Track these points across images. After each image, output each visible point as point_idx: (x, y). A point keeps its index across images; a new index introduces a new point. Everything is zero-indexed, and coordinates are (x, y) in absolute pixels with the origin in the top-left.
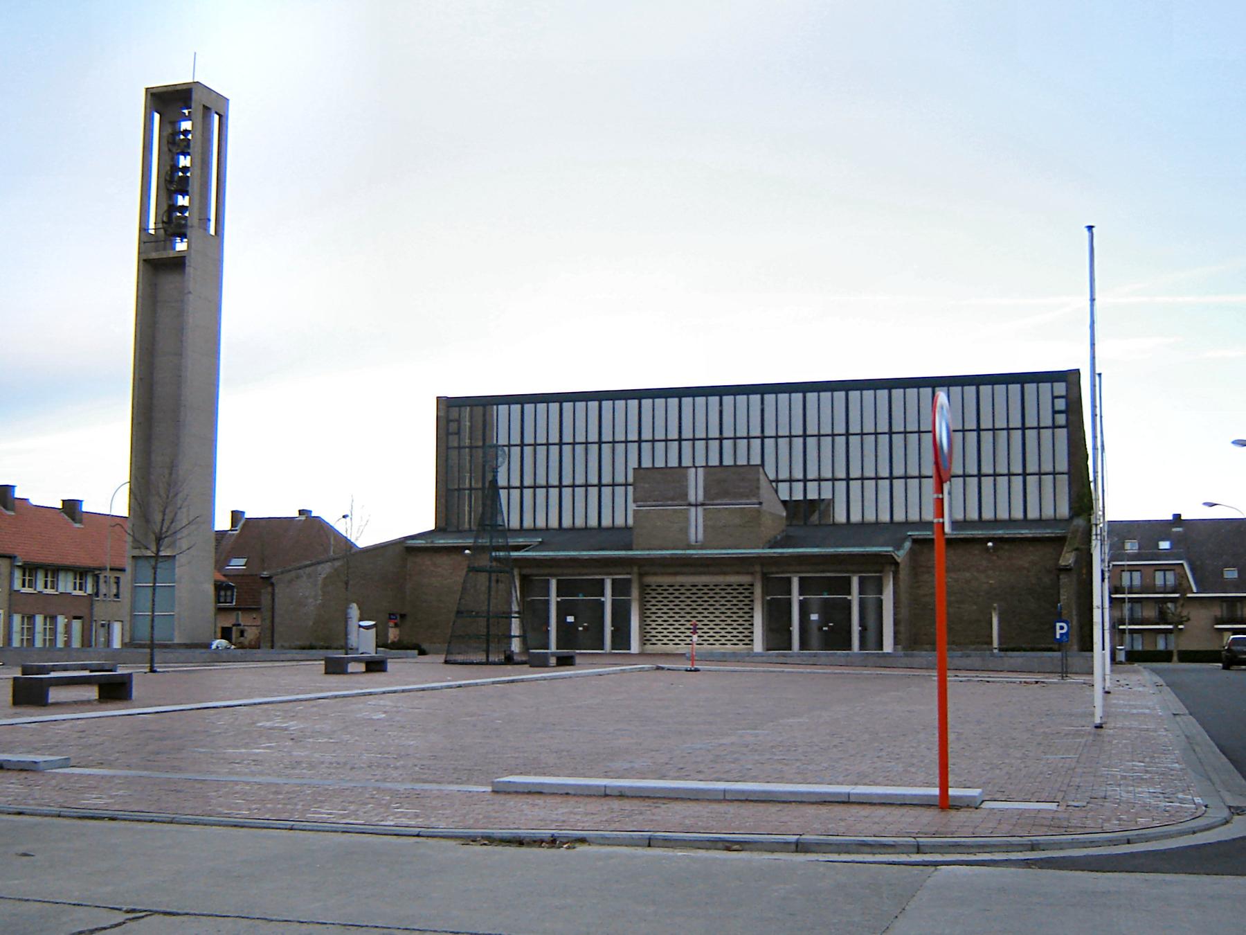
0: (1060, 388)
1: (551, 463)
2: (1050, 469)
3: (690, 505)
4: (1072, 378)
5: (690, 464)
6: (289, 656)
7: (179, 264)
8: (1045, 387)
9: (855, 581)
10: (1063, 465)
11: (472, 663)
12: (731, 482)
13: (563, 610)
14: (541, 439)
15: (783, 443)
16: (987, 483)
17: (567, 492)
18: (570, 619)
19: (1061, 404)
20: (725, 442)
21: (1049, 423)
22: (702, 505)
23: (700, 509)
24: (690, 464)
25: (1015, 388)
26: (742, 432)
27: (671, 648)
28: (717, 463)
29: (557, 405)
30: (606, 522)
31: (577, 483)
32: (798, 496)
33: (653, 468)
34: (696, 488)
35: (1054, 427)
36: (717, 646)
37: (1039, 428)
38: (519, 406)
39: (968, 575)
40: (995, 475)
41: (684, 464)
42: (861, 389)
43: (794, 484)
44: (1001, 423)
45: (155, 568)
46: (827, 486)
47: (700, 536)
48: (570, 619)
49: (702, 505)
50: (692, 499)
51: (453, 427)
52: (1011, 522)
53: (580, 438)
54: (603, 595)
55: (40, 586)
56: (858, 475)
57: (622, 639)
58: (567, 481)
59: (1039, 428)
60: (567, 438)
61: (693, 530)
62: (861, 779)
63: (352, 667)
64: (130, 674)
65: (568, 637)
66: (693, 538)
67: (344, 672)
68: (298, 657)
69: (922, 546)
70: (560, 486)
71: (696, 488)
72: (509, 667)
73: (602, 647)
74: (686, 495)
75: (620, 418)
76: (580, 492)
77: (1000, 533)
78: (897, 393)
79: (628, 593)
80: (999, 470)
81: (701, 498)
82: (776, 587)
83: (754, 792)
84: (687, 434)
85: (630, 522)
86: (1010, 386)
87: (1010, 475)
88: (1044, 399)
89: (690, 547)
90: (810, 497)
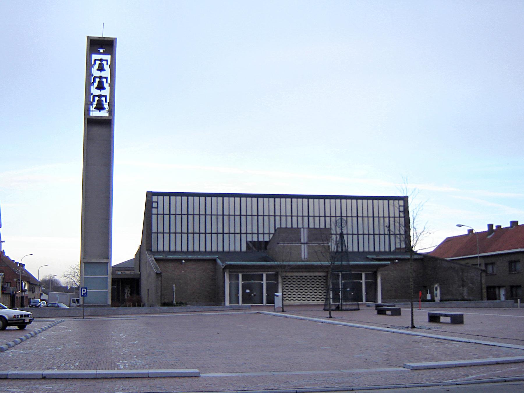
0: (402, 203)
1: (271, 225)
2: (180, 231)
3: (302, 243)
5: (301, 227)
6: (192, 310)
9: (240, 276)
10: (402, 232)
11: (348, 310)
12: (319, 235)
13: (244, 287)
15: (249, 218)
17: (377, 237)
18: (248, 291)
19: (402, 209)
20: (213, 216)
21: (398, 216)
22: (307, 243)
23: (305, 245)
24: (301, 227)
25: (272, 200)
26: (283, 213)
27: (292, 302)
28: (324, 227)
29: (186, 197)
30: (226, 249)
31: (213, 232)
32: (255, 239)
33: (281, 228)
34: (304, 236)
35: (400, 217)
36: (316, 301)
37: (314, 216)
38: (186, 197)
39: (387, 272)
40: (379, 234)
41: (299, 227)
42: (330, 199)
43: (254, 235)
44: (317, 214)
46: (249, 236)
47: (306, 257)
48: (248, 291)
49: (307, 243)
50: (302, 241)
52: (199, 252)
54: (361, 280)
56: (210, 231)
57: (271, 300)
58: (208, 231)
60: (208, 212)
61: (303, 254)
62: (173, 366)
63: (388, 312)
64: (463, 315)
65: (247, 299)
66: (303, 256)
67: (385, 314)
68: (197, 310)
69: (341, 263)
70: (374, 234)
71: (304, 236)
72: (337, 312)
73: (262, 303)
74: (300, 240)
75: (266, 205)
77: (190, 257)
78: (226, 199)
80: (183, 231)
81: (306, 241)
83: (125, 374)
85: (244, 249)
86: (183, 197)
87: (200, 233)
88: (395, 208)
89: (302, 261)
90: (260, 240)
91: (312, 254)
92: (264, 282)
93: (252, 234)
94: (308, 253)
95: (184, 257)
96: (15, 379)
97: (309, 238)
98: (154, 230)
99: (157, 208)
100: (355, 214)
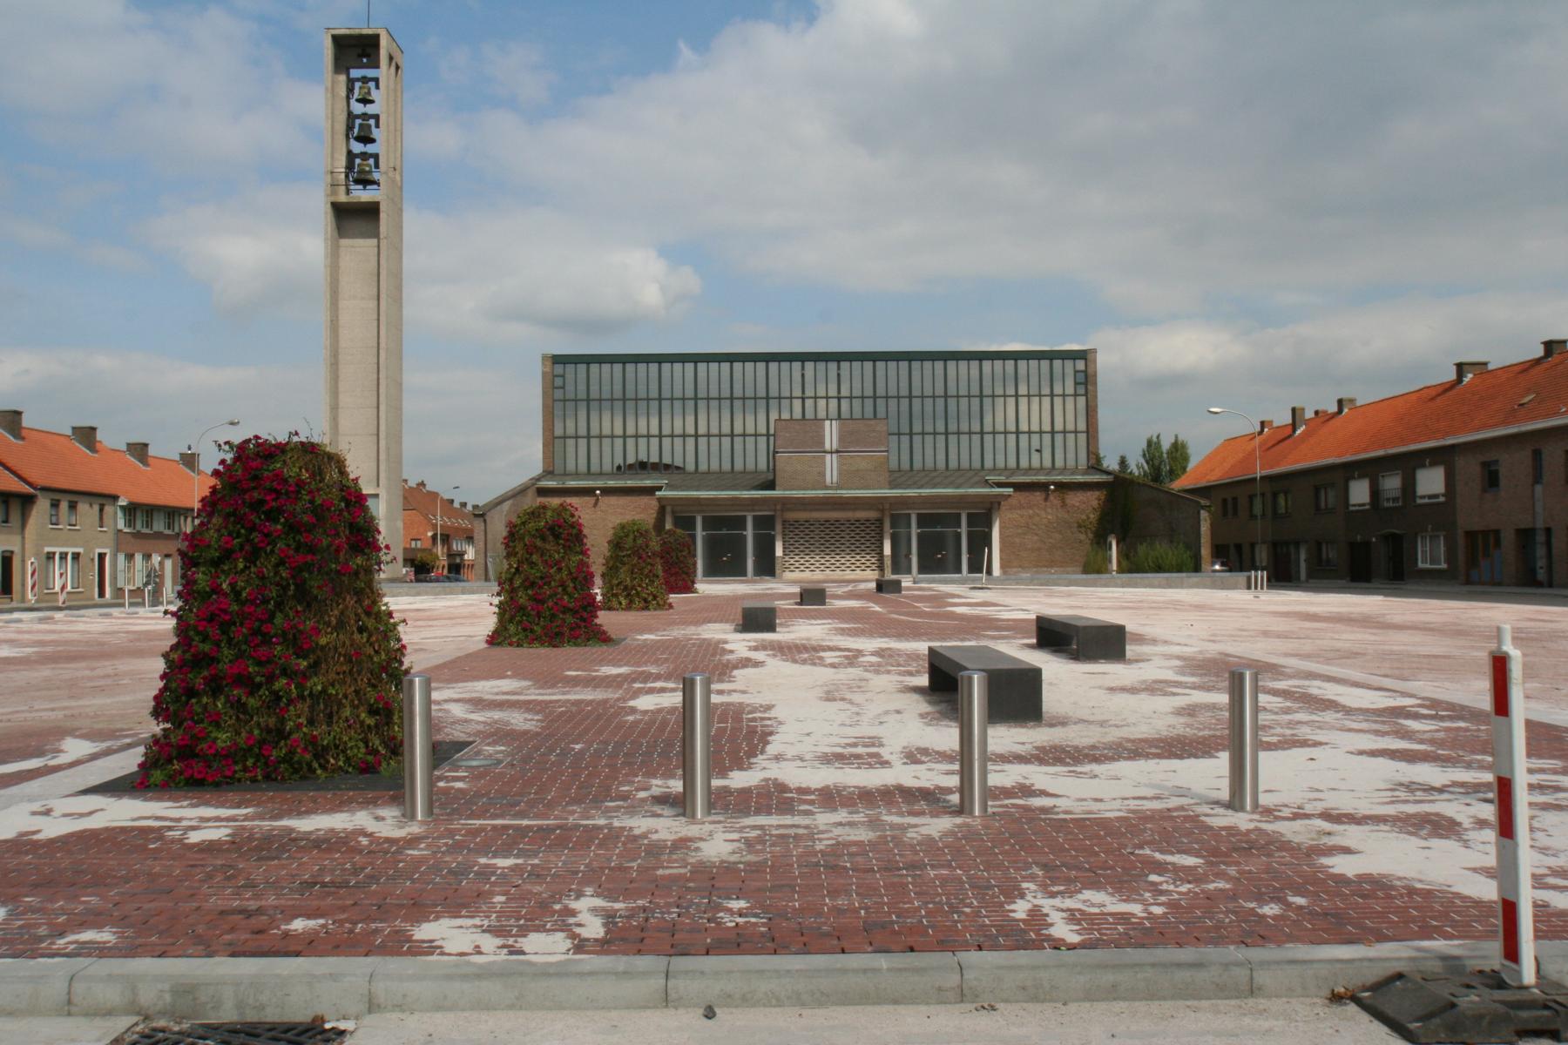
0: (1080, 365)
4: (1089, 357)
7: (370, 212)
8: (1069, 363)
10: (1082, 426)
14: (893, 392)
16: (953, 439)
19: (1081, 377)
30: (703, 467)
37: (923, 397)
45: (101, 510)
50: (827, 446)
51: (558, 382)
53: (714, 394)
55: (138, 526)
59: (923, 397)
63: (830, 657)
67: (821, 662)
73: (959, 571)
76: (606, 442)
79: (773, 529)
82: (899, 521)
84: (916, 392)
89: (827, 488)
91: (846, 478)
92: (964, 530)
93: (756, 435)
94: (840, 474)
95: (600, 483)
96: (1231, 610)
97: (841, 439)
98: (1082, 438)
99: (563, 387)
100: (940, 391)
